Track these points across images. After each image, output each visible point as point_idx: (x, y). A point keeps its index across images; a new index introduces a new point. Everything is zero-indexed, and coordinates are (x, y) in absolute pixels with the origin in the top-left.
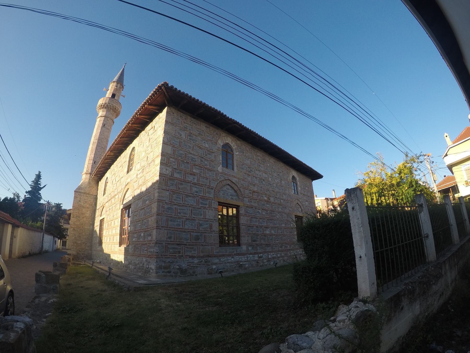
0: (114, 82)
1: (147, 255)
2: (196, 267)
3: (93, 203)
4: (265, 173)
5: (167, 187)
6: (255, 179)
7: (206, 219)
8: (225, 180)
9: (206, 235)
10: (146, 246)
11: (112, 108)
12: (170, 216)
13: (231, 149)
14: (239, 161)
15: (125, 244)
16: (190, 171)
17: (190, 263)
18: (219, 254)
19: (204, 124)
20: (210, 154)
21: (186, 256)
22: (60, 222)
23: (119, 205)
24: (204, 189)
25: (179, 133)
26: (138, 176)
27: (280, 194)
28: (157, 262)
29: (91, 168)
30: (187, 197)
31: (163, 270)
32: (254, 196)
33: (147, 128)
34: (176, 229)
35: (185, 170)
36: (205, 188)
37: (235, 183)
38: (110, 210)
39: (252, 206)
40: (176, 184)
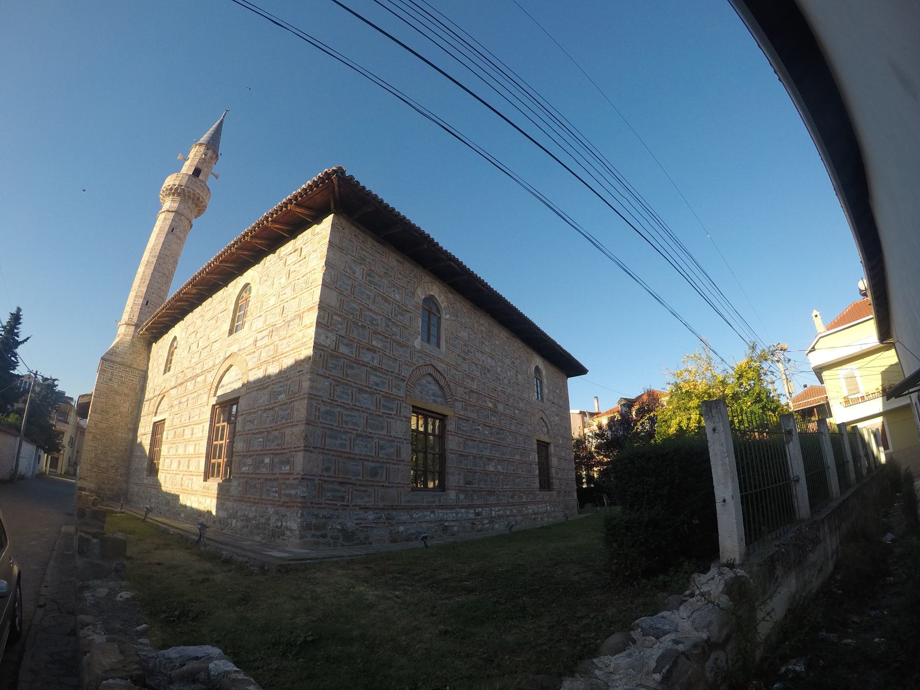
0: (201, 144)
1: (279, 501)
2: (370, 528)
3: (138, 387)
4: (492, 358)
5: (326, 372)
6: (475, 368)
7: (391, 436)
8: (425, 365)
9: (389, 468)
10: (276, 484)
11: (192, 196)
12: (330, 427)
13: (438, 307)
14: (449, 332)
15: (218, 475)
16: (367, 343)
17: (361, 519)
18: (411, 504)
19: (394, 255)
20: (402, 315)
21: (354, 506)
22: (51, 418)
23: (206, 396)
24: (389, 378)
25: (351, 268)
26: (258, 344)
27: (514, 399)
28: (304, 516)
29: (138, 314)
30: (359, 393)
31: (313, 532)
32: (471, 399)
33: (282, 249)
34: (339, 453)
35: (358, 340)
36: (391, 378)
37: (442, 372)
38: (181, 405)
39: (468, 417)
40: (341, 366)
